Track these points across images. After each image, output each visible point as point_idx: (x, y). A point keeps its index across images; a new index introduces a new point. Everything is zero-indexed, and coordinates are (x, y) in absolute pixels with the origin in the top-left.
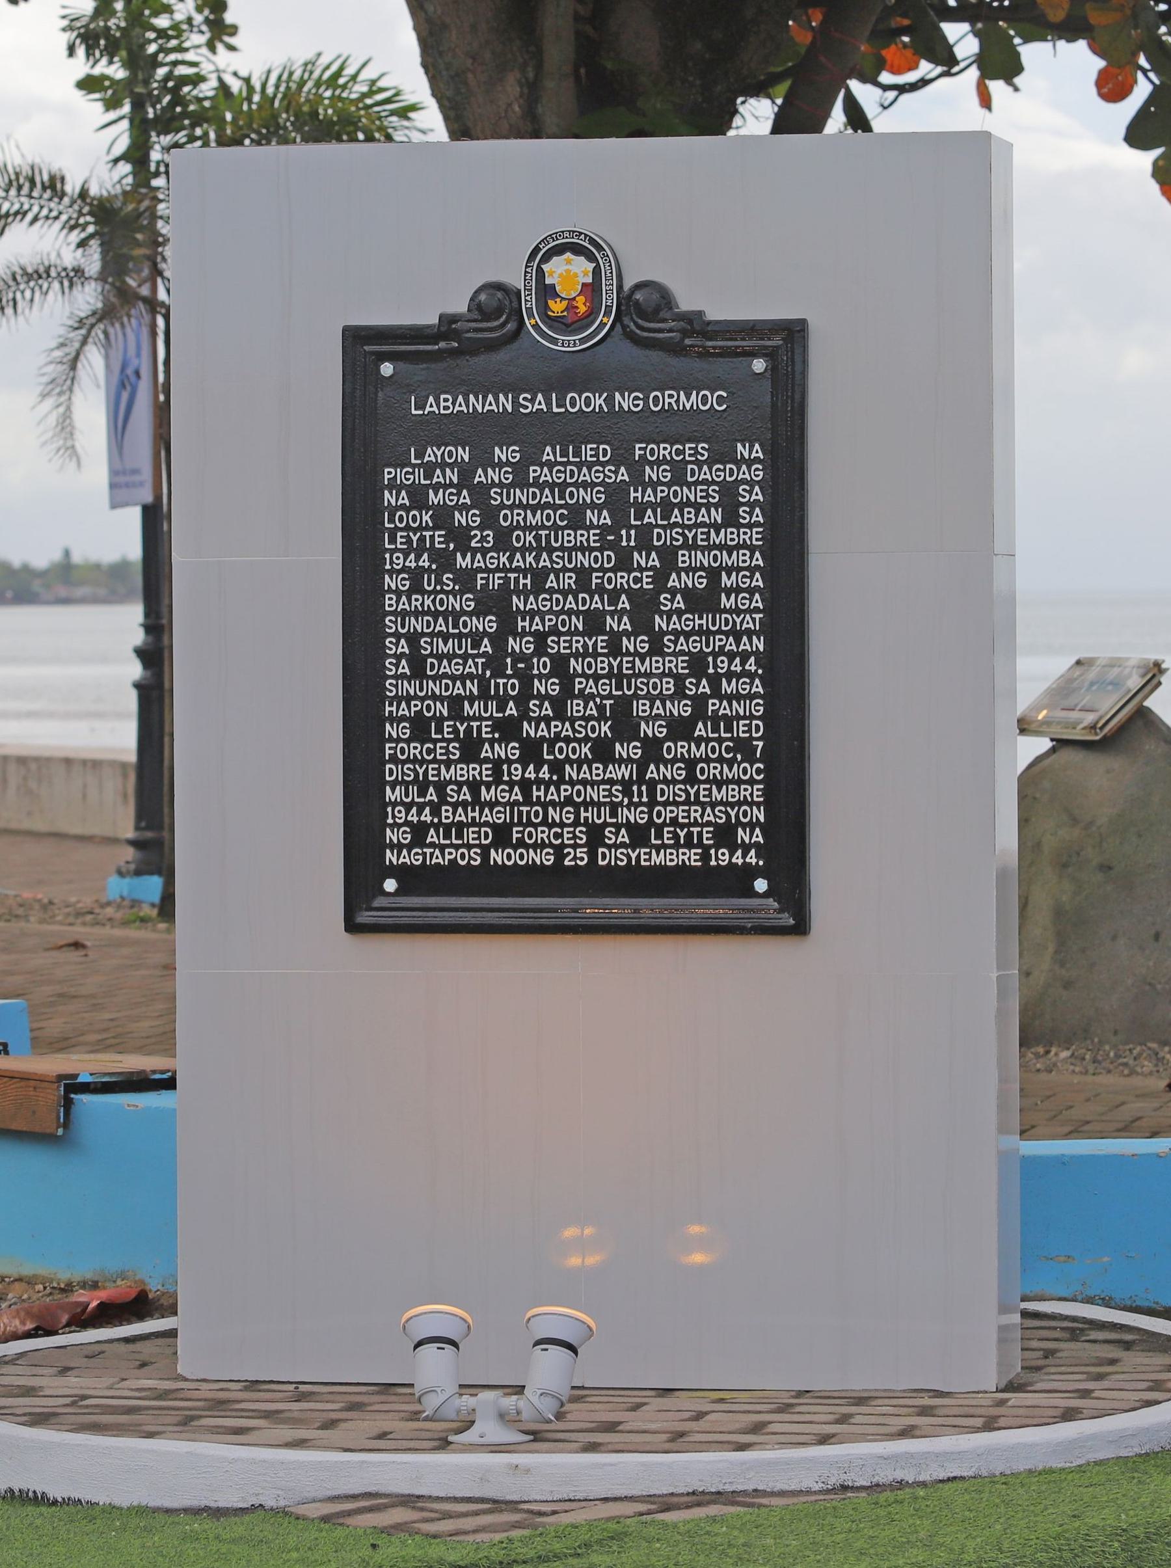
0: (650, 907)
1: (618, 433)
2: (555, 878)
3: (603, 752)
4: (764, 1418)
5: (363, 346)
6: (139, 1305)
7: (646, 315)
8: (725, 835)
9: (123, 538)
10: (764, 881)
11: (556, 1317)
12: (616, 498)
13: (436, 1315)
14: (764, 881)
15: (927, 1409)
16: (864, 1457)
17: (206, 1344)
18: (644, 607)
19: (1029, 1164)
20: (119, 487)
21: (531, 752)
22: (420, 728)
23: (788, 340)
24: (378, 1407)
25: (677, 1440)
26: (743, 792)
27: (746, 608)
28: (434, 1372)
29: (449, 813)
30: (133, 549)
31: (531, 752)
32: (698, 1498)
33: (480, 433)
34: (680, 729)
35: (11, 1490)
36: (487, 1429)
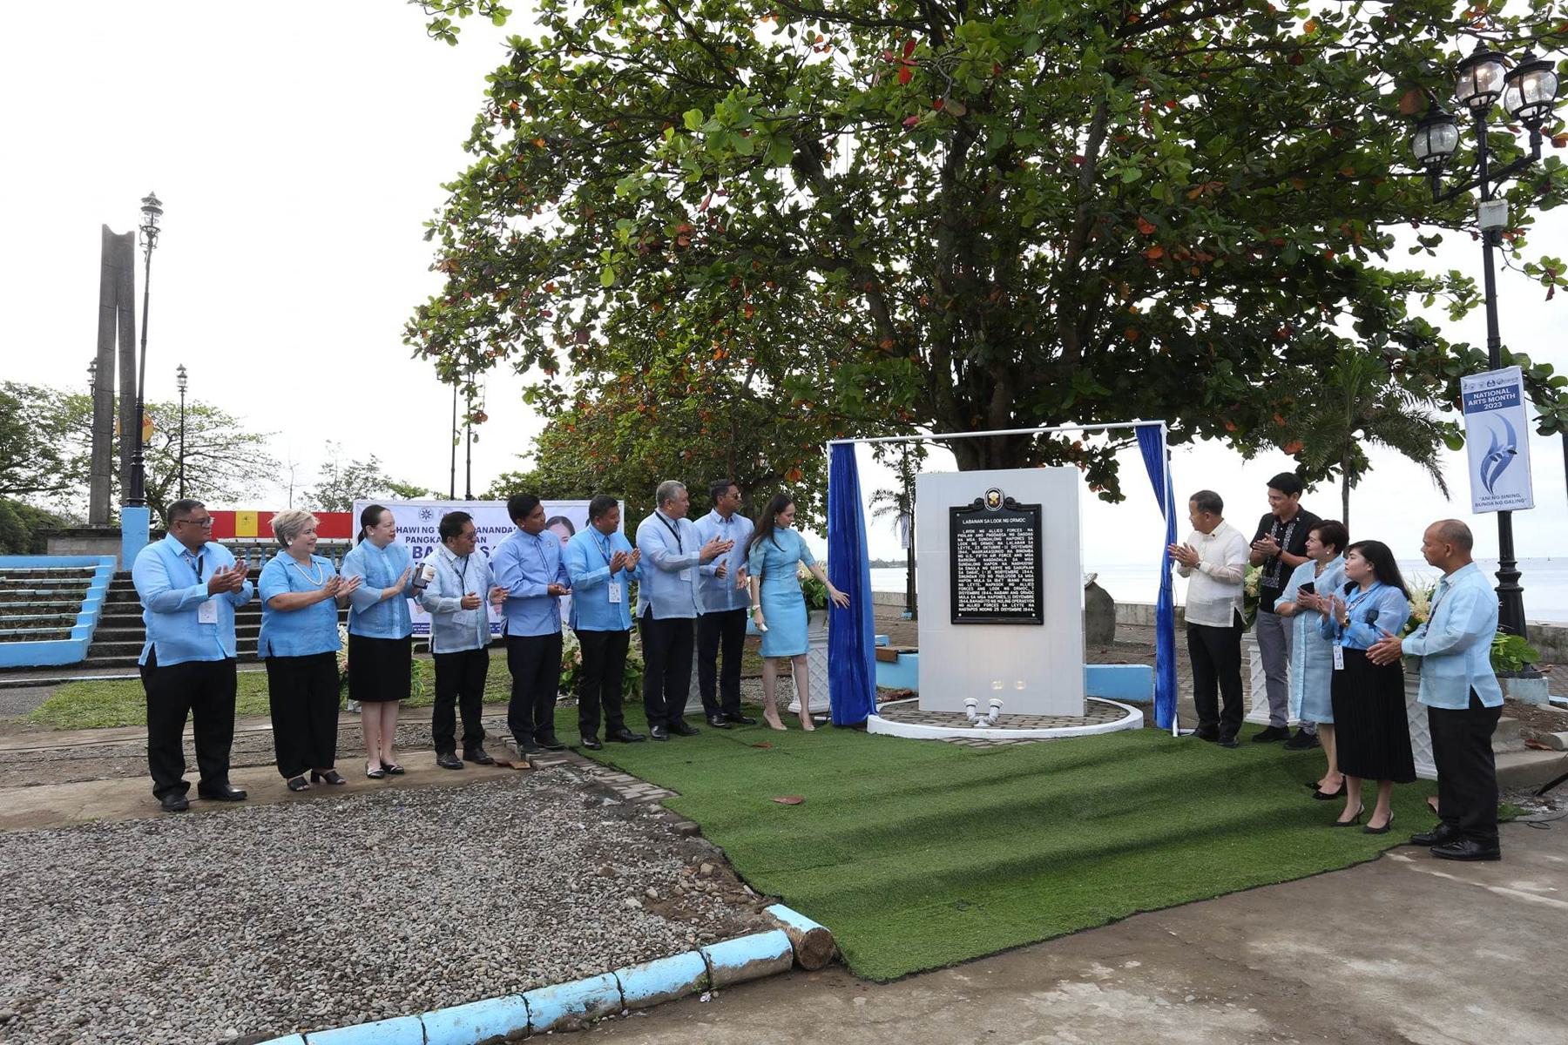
0: (1012, 619)
1: (1004, 527)
2: (993, 614)
3: (1002, 589)
4: (1037, 722)
5: (953, 510)
6: (911, 694)
7: (1009, 503)
8: (1026, 605)
9: (903, 556)
10: (1034, 616)
11: (994, 701)
12: (1004, 539)
13: (971, 700)
14: (1034, 616)
15: (1070, 721)
16: (1059, 731)
17: (925, 704)
18: (1009, 561)
19: (1089, 670)
20: (904, 545)
21: (987, 589)
22: (965, 584)
23: (1037, 509)
24: (958, 718)
25: (1020, 727)
26: (1030, 597)
27: (1030, 561)
28: (971, 712)
29: (972, 601)
30: (905, 558)
31: (987, 589)
32: (1026, 739)
33: (977, 527)
34: (1017, 584)
35: (144, 209)
36: (981, 724)
